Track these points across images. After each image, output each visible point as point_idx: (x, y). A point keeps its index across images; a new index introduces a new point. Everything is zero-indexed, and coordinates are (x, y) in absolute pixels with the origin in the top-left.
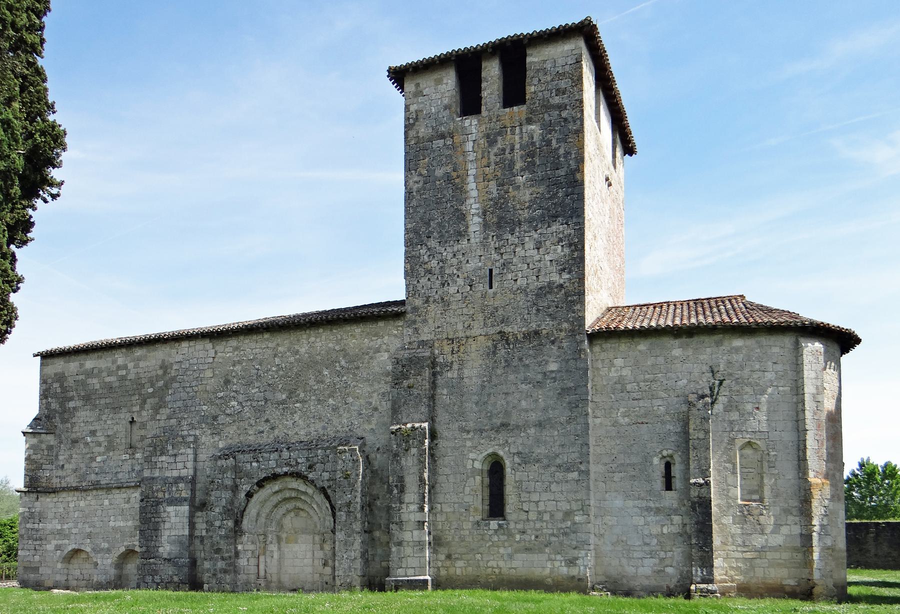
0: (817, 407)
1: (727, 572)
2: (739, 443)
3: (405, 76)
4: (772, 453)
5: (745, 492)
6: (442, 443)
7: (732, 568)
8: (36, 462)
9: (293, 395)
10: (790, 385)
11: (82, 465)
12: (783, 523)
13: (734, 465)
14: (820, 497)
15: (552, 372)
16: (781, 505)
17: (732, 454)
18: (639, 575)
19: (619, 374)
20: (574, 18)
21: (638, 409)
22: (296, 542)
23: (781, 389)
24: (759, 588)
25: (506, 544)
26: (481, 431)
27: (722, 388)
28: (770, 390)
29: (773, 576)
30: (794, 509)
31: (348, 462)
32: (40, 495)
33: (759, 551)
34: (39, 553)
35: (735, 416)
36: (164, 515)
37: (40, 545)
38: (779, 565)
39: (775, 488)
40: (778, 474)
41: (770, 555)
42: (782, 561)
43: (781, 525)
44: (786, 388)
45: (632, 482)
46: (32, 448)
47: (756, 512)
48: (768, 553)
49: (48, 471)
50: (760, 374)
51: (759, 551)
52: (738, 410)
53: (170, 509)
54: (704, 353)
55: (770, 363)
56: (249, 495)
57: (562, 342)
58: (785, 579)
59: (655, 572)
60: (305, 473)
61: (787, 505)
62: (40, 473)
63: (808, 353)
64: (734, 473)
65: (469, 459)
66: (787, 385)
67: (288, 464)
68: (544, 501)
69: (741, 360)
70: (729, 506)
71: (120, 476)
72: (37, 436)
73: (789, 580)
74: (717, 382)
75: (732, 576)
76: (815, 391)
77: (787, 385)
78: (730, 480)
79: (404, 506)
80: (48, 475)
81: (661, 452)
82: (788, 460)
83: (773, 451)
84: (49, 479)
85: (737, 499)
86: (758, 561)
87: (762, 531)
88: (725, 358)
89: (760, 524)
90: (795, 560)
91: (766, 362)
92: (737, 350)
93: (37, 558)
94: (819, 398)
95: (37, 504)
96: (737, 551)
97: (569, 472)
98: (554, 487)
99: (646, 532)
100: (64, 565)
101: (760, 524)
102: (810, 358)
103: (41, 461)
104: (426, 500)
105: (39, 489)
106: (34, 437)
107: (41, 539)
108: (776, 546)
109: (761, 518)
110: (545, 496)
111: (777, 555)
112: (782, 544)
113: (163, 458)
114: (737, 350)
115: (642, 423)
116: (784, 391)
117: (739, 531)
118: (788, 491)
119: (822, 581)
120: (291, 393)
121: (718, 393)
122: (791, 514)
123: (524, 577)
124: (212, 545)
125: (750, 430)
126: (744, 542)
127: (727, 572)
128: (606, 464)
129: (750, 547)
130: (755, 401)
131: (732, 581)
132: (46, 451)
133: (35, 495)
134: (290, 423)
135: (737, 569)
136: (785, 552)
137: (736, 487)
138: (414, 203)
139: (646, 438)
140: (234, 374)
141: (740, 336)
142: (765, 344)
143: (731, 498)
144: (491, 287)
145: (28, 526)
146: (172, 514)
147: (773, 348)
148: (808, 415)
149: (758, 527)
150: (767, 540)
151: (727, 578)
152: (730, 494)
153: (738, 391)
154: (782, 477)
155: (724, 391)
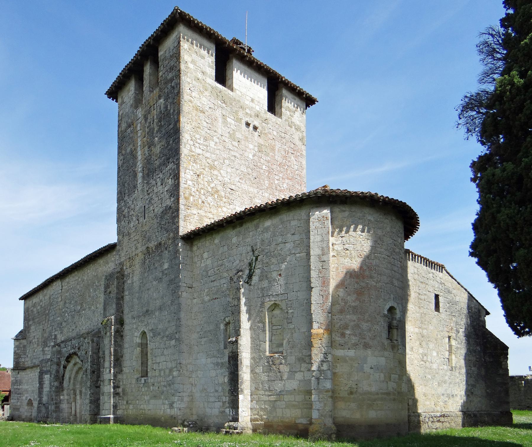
0: (322, 266)
1: (258, 412)
2: (267, 305)
3: (117, 94)
4: (290, 311)
5: (274, 346)
6: (126, 327)
7: (261, 409)
8: (18, 354)
10: (306, 251)
12: (298, 370)
13: (264, 323)
14: (321, 346)
15: (166, 269)
16: (296, 354)
17: (263, 315)
18: (213, 414)
19: (205, 264)
20: (165, 15)
21: (213, 288)
23: (298, 255)
24: (279, 426)
27: (258, 263)
28: (288, 259)
29: (288, 415)
30: (307, 358)
32: (20, 371)
33: (279, 395)
34: (20, 401)
35: (265, 284)
37: (20, 397)
38: (294, 406)
39: (291, 340)
40: (294, 328)
41: (287, 398)
42: (297, 403)
43: (296, 372)
44: (301, 255)
45: (210, 344)
46: (16, 347)
47: (277, 362)
48: (285, 396)
49: (23, 359)
50: (282, 245)
51: (279, 395)
52: (267, 279)
54: (248, 236)
55: (289, 235)
56: (65, 367)
57: (170, 247)
58: (299, 418)
59: (220, 412)
61: (301, 354)
62: (20, 360)
63: (314, 221)
64: (264, 331)
65: (134, 336)
66: (303, 251)
69: (269, 237)
70: (261, 358)
72: (19, 341)
73: (302, 420)
74: (254, 258)
75: (261, 416)
76: (320, 252)
77: (303, 251)
78: (261, 337)
79: (105, 370)
80: (23, 361)
81: (224, 319)
82: (303, 316)
83: (291, 309)
84: (24, 362)
85: (266, 352)
86: (278, 403)
87: (282, 378)
88: (260, 238)
89: (280, 372)
90: (307, 402)
91: (286, 234)
92: (267, 229)
93: (19, 404)
94: (324, 258)
95: (19, 376)
96: (265, 395)
97: (171, 341)
98: (166, 352)
99: (216, 382)
100: (29, 407)
101: (280, 372)
102: (317, 224)
103: (21, 354)
104: (112, 365)
105: (18, 368)
106: (18, 341)
107: (20, 394)
108: (292, 390)
109: (281, 366)
110: (163, 358)
111: (291, 398)
112: (296, 388)
114: (267, 229)
115: (216, 299)
116: (300, 257)
117: (266, 378)
118: (302, 343)
119: (320, 420)
121: (254, 267)
122: (305, 361)
123: (153, 416)
125: (275, 294)
126: (269, 388)
127: (258, 412)
128: (198, 332)
129: (274, 392)
130: (278, 269)
131: (261, 420)
132: (22, 348)
133: (17, 371)
135: (264, 410)
136: (299, 395)
137: (265, 342)
138: (120, 174)
139: (217, 309)
141: (270, 218)
142: (285, 219)
143: (262, 351)
144: (145, 219)
145: (15, 387)
147: (292, 222)
148: (314, 274)
149: (279, 374)
150: (284, 385)
151: (258, 417)
152: (261, 349)
153: (267, 263)
154: (297, 331)
155: (259, 265)
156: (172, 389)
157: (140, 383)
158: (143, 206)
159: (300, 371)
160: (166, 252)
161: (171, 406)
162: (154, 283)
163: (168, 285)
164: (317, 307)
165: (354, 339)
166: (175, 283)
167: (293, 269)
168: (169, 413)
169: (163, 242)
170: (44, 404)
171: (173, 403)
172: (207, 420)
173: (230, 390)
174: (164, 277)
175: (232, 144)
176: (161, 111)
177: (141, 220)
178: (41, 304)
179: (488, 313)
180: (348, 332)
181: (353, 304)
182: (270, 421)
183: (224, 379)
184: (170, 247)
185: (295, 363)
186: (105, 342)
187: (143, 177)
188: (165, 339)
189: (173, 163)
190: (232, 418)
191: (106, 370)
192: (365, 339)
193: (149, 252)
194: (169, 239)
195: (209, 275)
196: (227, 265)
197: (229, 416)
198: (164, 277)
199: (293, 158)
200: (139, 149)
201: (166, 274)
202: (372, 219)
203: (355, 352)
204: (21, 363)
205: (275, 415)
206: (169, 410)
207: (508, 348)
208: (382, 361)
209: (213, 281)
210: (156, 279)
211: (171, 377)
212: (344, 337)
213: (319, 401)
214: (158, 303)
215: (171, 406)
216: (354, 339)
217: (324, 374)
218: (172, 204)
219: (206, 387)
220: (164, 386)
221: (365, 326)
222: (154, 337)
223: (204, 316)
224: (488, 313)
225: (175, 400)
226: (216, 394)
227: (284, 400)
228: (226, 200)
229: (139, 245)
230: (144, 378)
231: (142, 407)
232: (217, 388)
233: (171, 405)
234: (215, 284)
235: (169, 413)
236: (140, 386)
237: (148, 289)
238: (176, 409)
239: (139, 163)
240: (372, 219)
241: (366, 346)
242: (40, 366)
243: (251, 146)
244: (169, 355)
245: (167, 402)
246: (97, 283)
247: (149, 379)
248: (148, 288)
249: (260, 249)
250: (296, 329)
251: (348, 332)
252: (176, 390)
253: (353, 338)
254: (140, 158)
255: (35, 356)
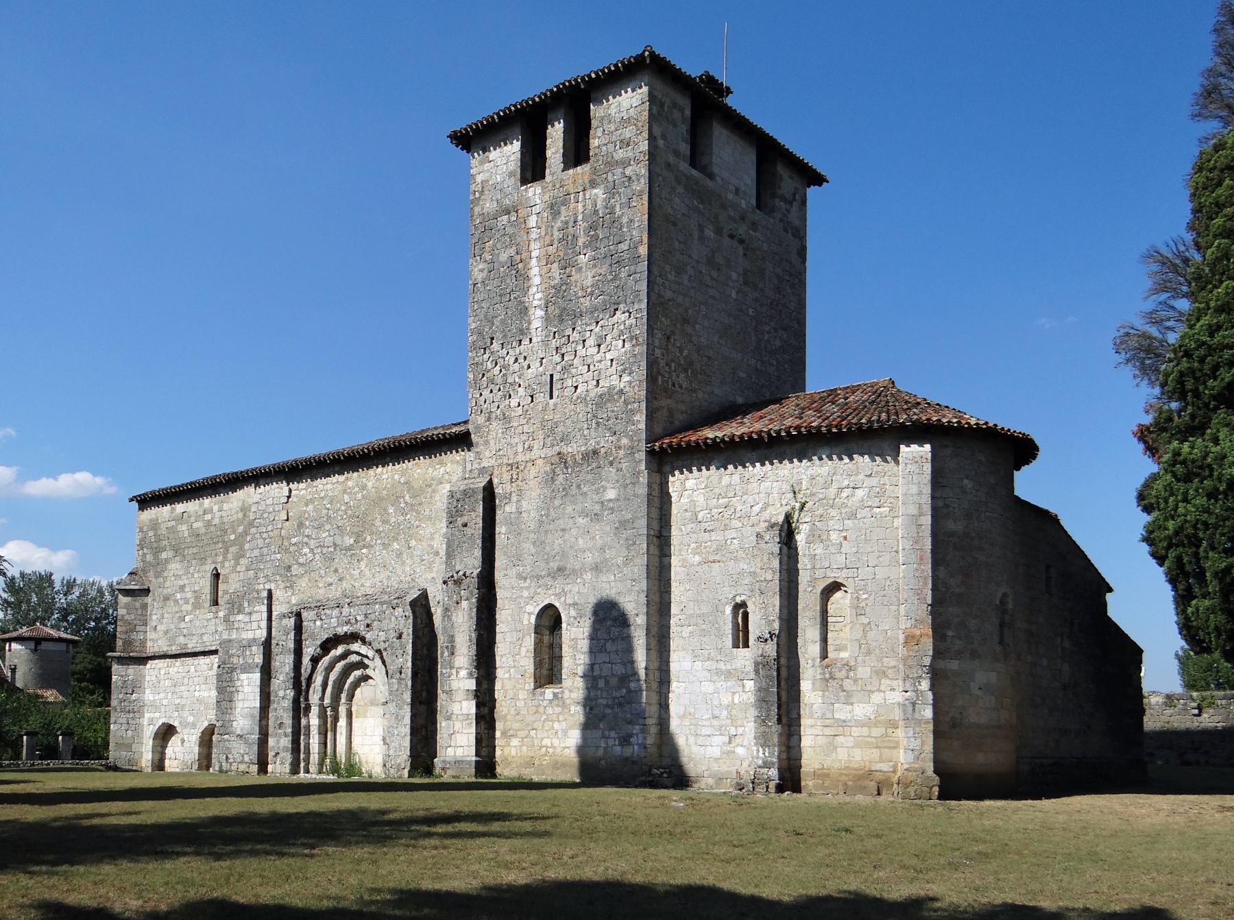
9: (360, 539)
11: (172, 626)
15: (610, 500)
22: (366, 717)
24: (841, 774)
25: (561, 718)
26: (538, 577)
29: (858, 758)
31: (400, 619)
36: (238, 683)
40: (869, 623)
43: (873, 692)
53: (244, 676)
56: (315, 661)
60: (364, 633)
67: (348, 623)
68: (600, 664)
71: (205, 638)
79: (454, 671)
86: (840, 739)
98: (609, 646)
113: (240, 617)
120: (359, 537)
122: (887, 676)
124: (277, 718)
130: (841, 529)
134: (356, 573)
140: (306, 516)
144: (551, 397)
146: (245, 683)
156: (626, 712)
157: (541, 698)
158: (548, 373)
159: (879, 690)
160: (611, 469)
161: (625, 740)
162: (580, 520)
163: (617, 528)
164: (911, 594)
165: (958, 644)
166: (634, 528)
167: (868, 531)
168: (620, 753)
169: (603, 450)
170: (241, 736)
171: (631, 735)
172: (695, 765)
173: (758, 716)
174: (606, 513)
175: (711, 276)
176: (596, 212)
177: (541, 398)
178: (208, 517)
179: (1110, 590)
180: (950, 633)
181: (957, 590)
182: (825, 767)
183: (733, 699)
184: (620, 463)
185: (871, 678)
186: (454, 618)
187: (547, 319)
188: (609, 623)
189: (627, 314)
190: (764, 762)
191: (457, 672)
192: (972, 643)
193: (565, 463)
194: (620, 448)
195: (700, 518)
196: (739, 508)
197: (757, 758)
198: (606, 513)
199: (789, 290)
200: (534, 262)
201: (612, 509)
202: (983, 459)
203: (959, 664)
204: (137, 644)
205: (834, 758)
206: (618, 749)
207: (1142, 651)
208: (993, 677)
209: (709, 531)
210: (584, 513)
211: (624, 691)
212: (945, 641)
213: (915, 737)
214: (590, 558)
215: (625, 740)
216: (958, 644)
217: (922, 696)
218: (625, 387)
219: (692, 710)
220: (607, 706)
221: (972, 623)
222: (581, 617)
223: (688, 588)
224: (1110, 590)
225: (634, 732)
226: (715, 723)
227: (850, 735)
228: (702, 377)
229: (536, 445)
230: (551, 690)
231: (546, 742)
232: (716, 712)
233: (625, 740)
234: (714, 536)
235: (620, 753)
236: (540, 705)
237: (563, 530)
238: (636, 747)
239: (534, 290)
240: (983, 459)
241: (974, 655)
242: (220, 654)
243: (734, 276)
244: (620, 654)
245: (613, 734)
246: (407, 498)
247: (567, 692)
248: (563, 527)
249: (808, 492)
250: (873, 626)
251: (950, 633)
252: (638, 714)
253: (958, 642)
254: (536, 280)
255: (185, 630)
